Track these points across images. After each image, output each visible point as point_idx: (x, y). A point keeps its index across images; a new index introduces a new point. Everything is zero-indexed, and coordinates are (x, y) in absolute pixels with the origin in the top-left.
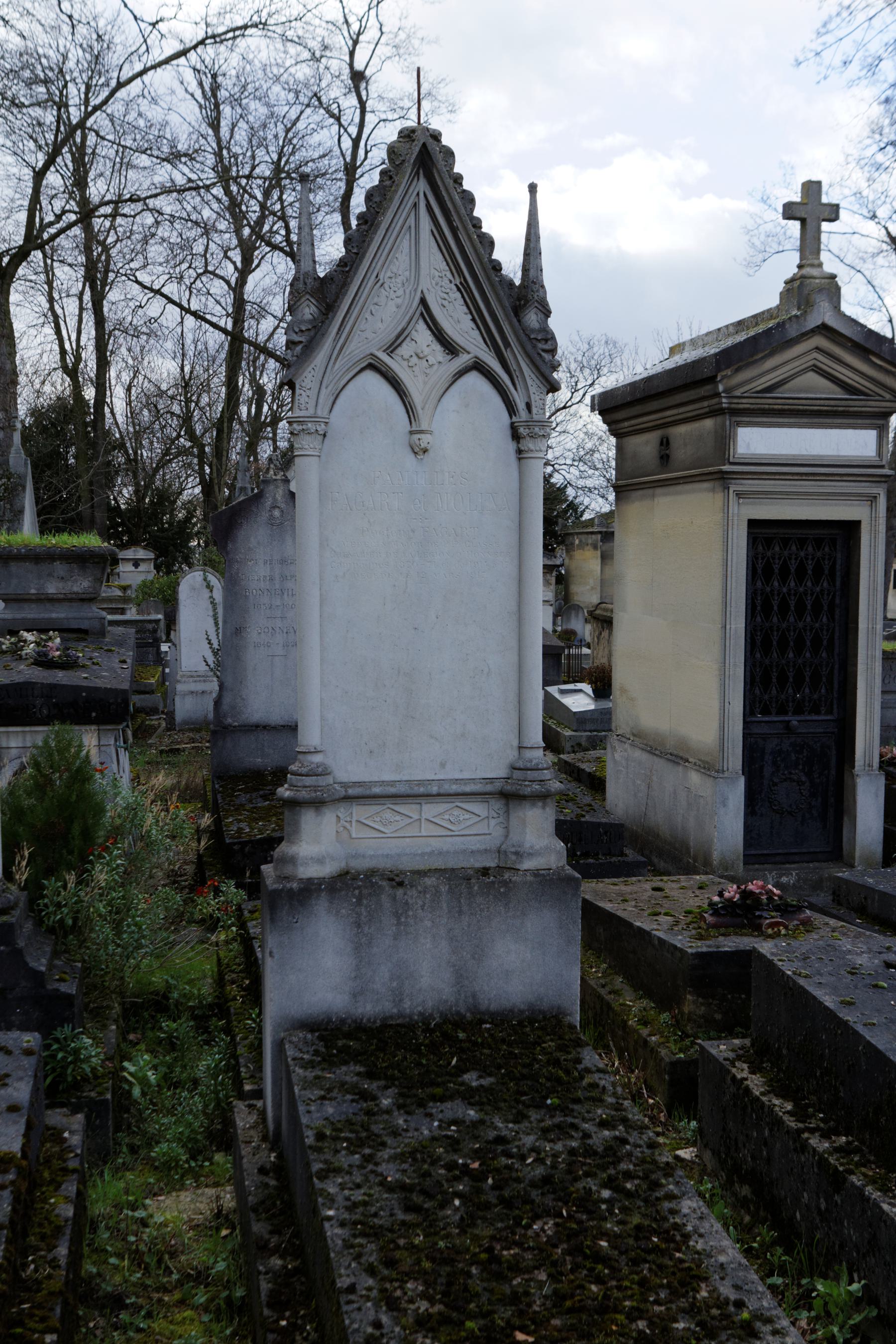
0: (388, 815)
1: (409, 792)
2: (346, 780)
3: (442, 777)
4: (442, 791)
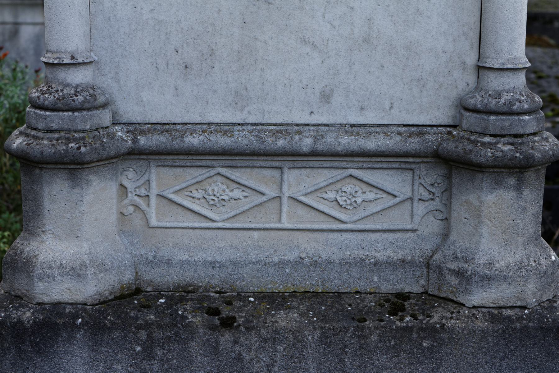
0: (218, 187)
1: (256, 145)
2: (139, 119)
3: (323, 120)
4: (320, 147)
